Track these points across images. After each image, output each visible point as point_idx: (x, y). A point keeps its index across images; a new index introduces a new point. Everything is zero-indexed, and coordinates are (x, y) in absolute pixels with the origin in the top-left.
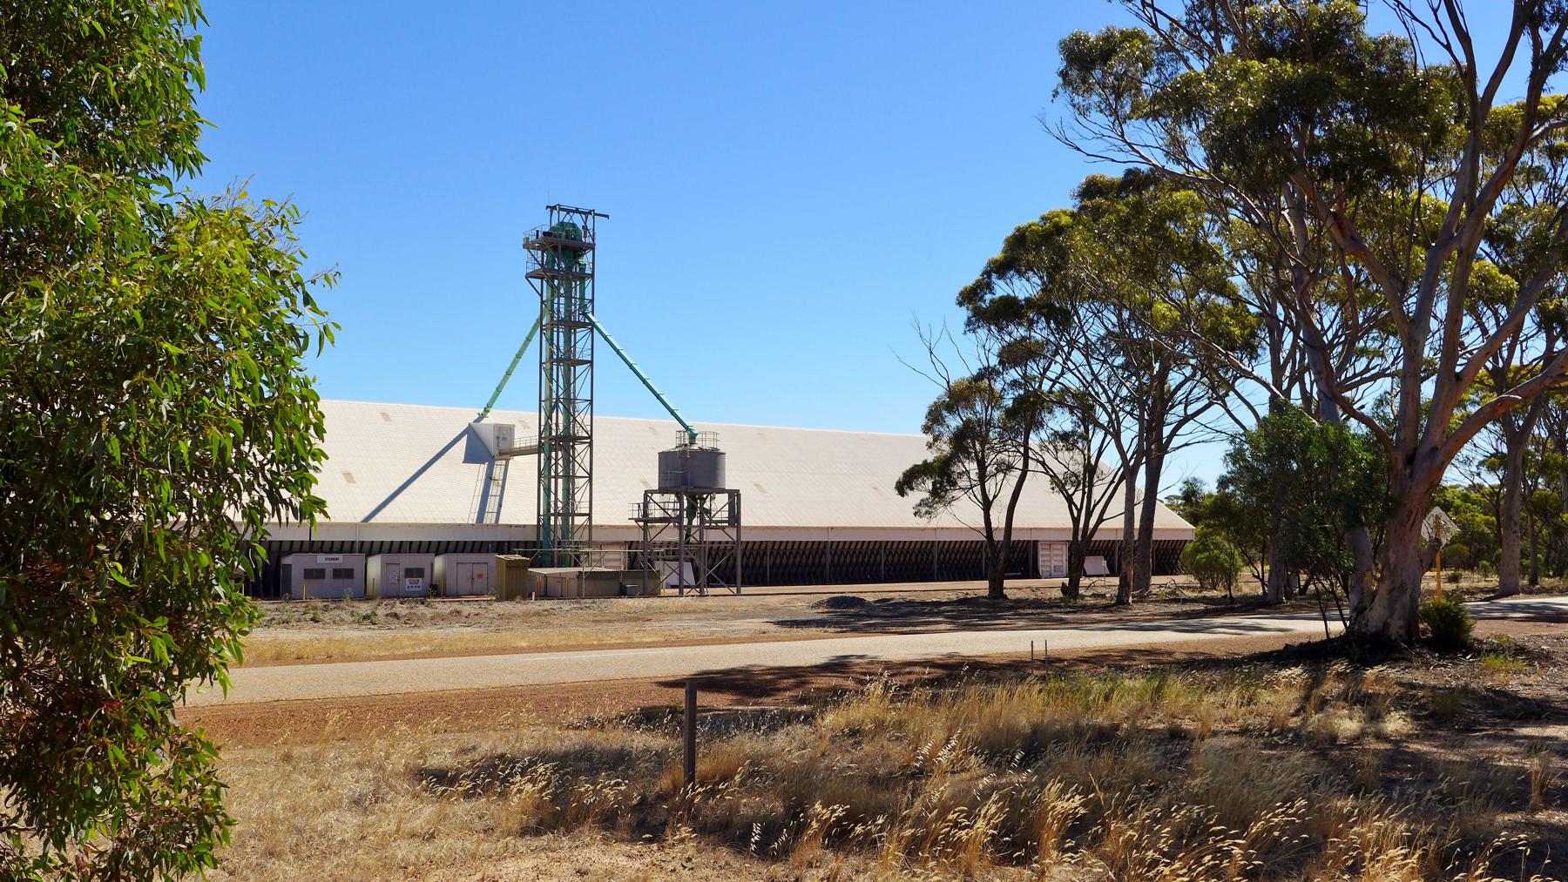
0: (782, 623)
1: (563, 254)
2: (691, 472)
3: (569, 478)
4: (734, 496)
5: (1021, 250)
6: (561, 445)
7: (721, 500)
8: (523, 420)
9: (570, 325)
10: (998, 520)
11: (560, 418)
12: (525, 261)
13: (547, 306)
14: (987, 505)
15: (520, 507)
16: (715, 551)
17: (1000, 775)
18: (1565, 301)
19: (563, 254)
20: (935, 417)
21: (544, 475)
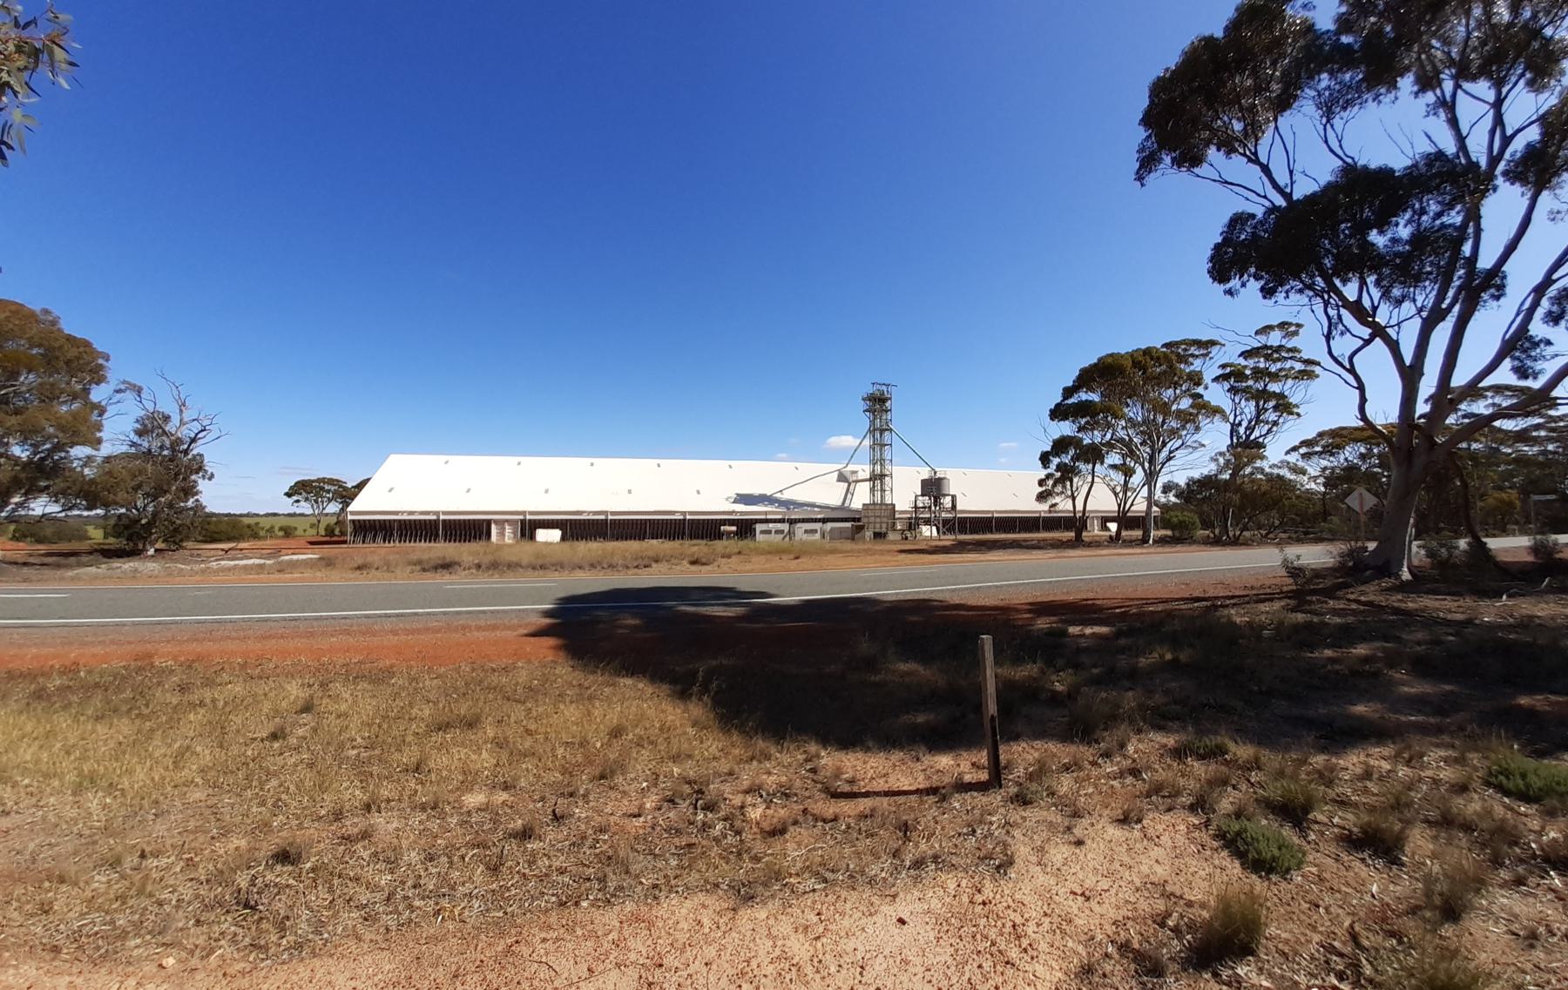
0: (311, 543)
1: (877, 403)
2: (933, 487)
3: (883, 491)
4: (954, 497)
5: (1087, 378)
6: (877, 478)
7: (948, 499)
8: (864, 471)
9: (882, 431)
10: (1079, 507)
11: (878, 468)
12: (862, 406)
13: (873, 422)
14: (1074, 499)
15: (861, 497)
16: (946, 522)
17: (1201, 732)
18: (1567, 342)
19: (877, 403)
20: (1045, 459)
21: (872, 490)
